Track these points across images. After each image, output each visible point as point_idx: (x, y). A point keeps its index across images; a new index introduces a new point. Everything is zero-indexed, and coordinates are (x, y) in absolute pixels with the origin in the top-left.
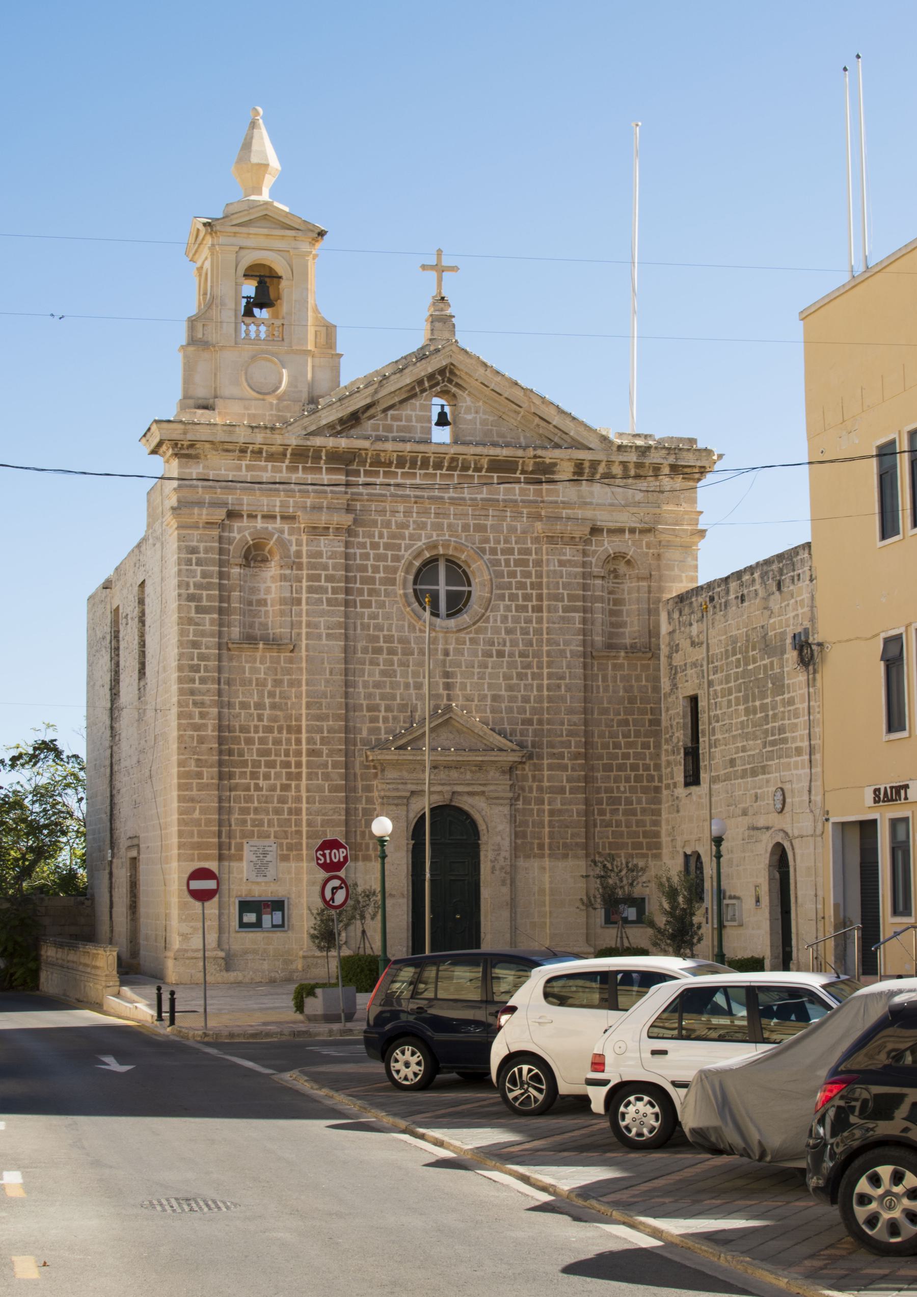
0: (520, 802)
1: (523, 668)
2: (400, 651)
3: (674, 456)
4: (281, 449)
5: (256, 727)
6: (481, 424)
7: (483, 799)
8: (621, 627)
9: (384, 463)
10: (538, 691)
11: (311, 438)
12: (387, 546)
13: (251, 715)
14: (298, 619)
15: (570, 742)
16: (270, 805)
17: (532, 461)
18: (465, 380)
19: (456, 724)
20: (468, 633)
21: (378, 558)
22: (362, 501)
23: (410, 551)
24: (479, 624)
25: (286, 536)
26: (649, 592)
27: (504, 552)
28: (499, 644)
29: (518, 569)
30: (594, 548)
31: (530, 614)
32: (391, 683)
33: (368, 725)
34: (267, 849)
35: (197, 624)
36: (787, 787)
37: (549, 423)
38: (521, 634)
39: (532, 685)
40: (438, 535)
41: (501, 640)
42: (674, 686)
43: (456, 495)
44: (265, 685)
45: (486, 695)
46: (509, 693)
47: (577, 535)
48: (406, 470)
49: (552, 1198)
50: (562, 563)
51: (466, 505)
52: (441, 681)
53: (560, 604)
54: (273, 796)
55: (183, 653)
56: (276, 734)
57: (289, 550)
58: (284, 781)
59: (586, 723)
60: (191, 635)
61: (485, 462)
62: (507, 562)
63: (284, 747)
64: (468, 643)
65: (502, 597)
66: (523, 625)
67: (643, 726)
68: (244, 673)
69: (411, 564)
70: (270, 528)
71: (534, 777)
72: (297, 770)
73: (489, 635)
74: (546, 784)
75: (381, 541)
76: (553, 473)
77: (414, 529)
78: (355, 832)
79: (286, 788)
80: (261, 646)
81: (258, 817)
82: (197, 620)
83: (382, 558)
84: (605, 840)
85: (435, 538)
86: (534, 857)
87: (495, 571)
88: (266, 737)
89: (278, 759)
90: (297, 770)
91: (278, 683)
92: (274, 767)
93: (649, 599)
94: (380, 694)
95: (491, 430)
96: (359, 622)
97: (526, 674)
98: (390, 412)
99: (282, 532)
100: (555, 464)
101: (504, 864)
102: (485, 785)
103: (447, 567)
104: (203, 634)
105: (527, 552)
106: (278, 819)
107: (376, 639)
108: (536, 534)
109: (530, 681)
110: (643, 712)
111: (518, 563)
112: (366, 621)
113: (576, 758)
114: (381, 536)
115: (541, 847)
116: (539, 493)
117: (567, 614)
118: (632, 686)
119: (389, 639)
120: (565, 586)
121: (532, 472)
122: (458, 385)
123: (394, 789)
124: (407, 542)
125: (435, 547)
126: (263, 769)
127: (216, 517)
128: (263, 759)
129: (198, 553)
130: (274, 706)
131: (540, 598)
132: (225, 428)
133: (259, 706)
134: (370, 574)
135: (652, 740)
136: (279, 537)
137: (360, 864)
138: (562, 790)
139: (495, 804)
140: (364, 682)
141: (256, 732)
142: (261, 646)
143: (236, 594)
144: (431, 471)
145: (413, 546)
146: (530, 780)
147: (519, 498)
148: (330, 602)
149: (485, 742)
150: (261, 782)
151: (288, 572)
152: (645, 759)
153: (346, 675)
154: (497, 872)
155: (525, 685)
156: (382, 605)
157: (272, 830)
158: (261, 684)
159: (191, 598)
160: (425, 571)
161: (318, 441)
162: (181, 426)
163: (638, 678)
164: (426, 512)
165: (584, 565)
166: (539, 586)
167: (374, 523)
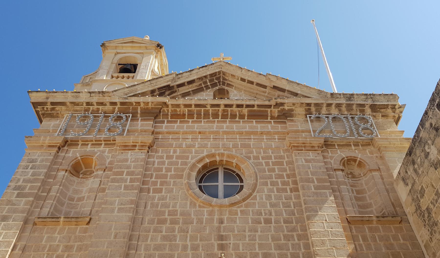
1: (288, 231)
2: (181, 221)
8: (368, 208)
9: (180, 115)
10: (305, 248)
11: (129, 98)
17: (276, 110)
20: (238, 207)
21: (171, 164)
23: (195, 160)
24: (248, 201)
25: (106, 154)
28: (266, 214)
30: (330, 155)
32: (170, 245)
38: (284, 207)
39: (299, 245)
40: (215, 150)
41: (267, 212)
44: (56, 250)
45: (258, 254)
46: (278, 252)
49: (395, 177)
50: (307, 161)
52: (216, 244)
57: (106, 161)
61: (245, 111)
65: (266, 184)
69: (194, 165)
73: (257, 208)
76: (292, 116)
82: (14, 202)
97: (293, 236)
103: (225, 173)
105: (281, 157)
112: (156, 201)
114: (175, 152)
118: (392, 245)
122: (229, 85)
125: (213, 155)
131: (295, 183)
132: (73, 94)
143: (55, 188)
155: (293, 245)
156: (171, 191)
163: (395, 238)
166: (294, 175)
167: (171, 146)
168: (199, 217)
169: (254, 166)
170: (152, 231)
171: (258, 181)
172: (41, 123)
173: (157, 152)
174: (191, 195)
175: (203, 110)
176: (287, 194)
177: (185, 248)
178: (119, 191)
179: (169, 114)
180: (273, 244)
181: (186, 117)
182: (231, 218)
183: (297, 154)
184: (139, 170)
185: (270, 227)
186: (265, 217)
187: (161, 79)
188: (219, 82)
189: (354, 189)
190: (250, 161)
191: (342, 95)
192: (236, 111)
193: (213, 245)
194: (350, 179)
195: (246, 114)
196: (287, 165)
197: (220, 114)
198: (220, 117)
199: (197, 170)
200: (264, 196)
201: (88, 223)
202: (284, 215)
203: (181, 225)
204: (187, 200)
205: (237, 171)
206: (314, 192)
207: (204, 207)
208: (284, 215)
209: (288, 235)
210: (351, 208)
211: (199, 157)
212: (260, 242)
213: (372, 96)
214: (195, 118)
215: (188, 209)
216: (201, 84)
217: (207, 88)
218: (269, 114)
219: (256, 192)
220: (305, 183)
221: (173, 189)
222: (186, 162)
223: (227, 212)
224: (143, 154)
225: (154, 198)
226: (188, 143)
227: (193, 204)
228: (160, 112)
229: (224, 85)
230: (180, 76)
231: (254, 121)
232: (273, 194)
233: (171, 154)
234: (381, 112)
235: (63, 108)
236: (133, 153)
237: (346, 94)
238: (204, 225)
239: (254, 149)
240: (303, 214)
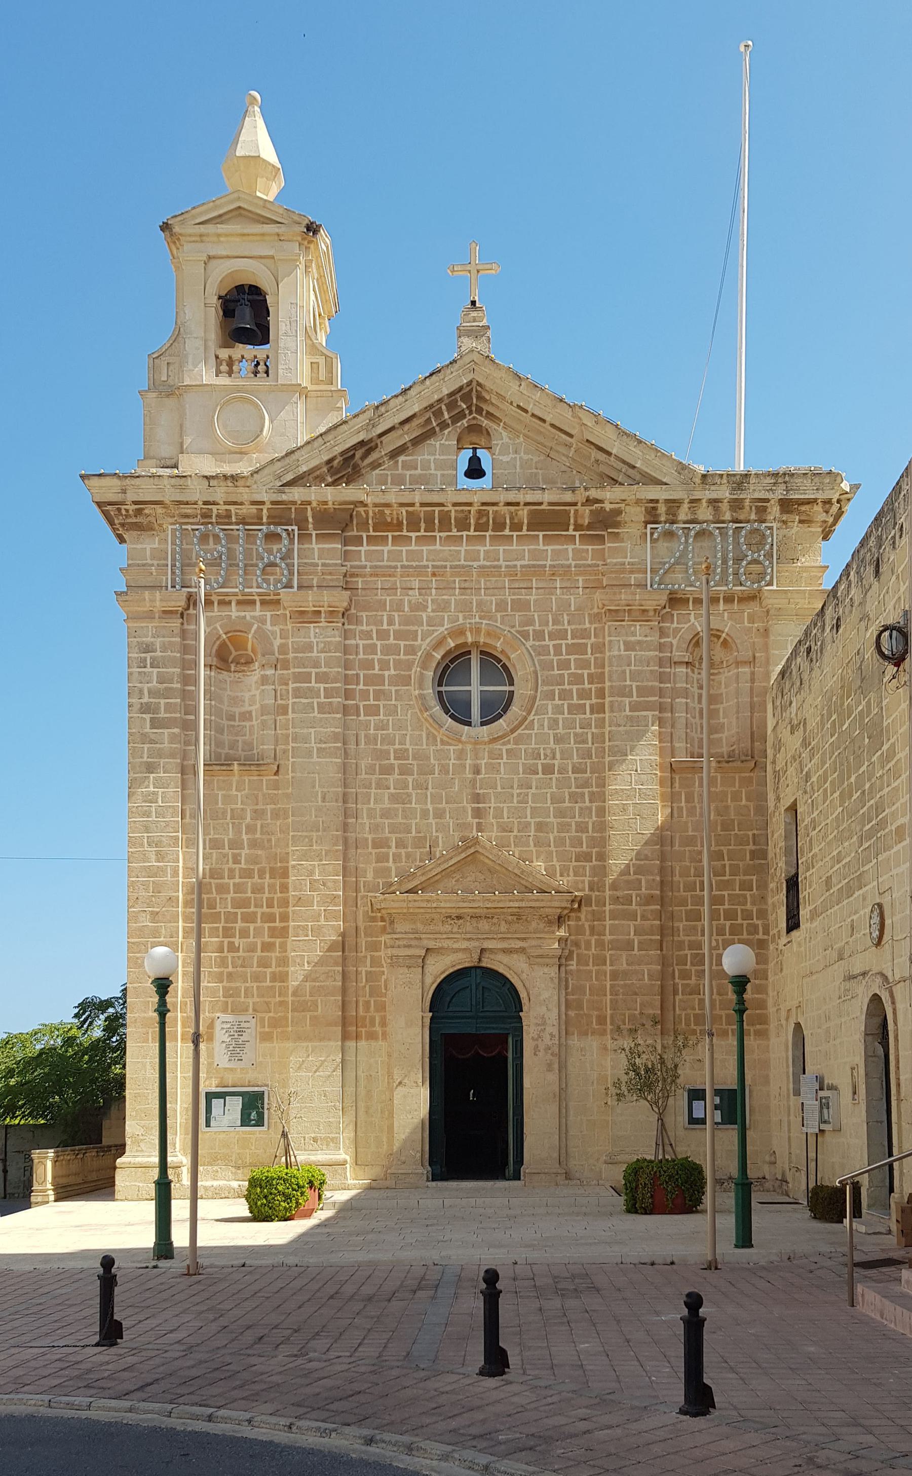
0: (574, 963)
3: (783, 486)
4: (253, 509)
5: (231, 871)
6: (521, 467)
7: (522, 958)
10: (597, 816)
11: (287, 489)
12: (399, 635)
13: (225, 855)
14: (284, 732)
15: (640, 881)
16: (249, 970)
17: (587, 510)
18: (498, 407)
19: (487, 861)
20: (504, 744)
21: (387, 650)
22: (365, 576)
24: (519, 731)
25: (268, 626)
26: (753, 680)
27: (552, 636)
28: (546, 756)
29: (572, 657)
31: (588, 715)
33: (374, 865)
34: (243, 1025)
35: (152, 742)
36: (886, 900)
37: (609, 454)
39: (590, 809)
40: (465, 618)
41: (548, 752)
42: (778, 799)
43: (488, 564)
44: (243, 818)
45: (530, 823)
46: (559, 820)
47: (650, 605)
48: (422, 533)
50: (629, 646)
51: (500, 576)
52: (469, 807)
53: (627, 700)
54: (252, 958)
55: (136, 779)
56: (256, 879)
57: (272, 644)
58: (267, 939)
59: (663, 857)
60: (145, 756)
61: (524, 514)
62: (557, 648)
63: (267, 895)
64: (505, 757)
65: (550, 696)
66: (578, 730)
67: (743, 859)
68: (217, 804)
69: (428, 656)
70: (248, 618)
71: (592, 928)
72: (283, 924)
74: (608, 937)
75: (391, 627)
76: (617, 525)
77: (433, 611)
78: (357, 1002)
79: (267, 947)
80: (236, 767)
81: (233, 985)
82: (153, 737)
83: (396, 650)
84: (689, 1011)
85: (461, 621)
86: (593, 1033)
87: (540, 661)
88: (244, 883)
89: (259, 910)
90: (283, 924)
91: (258, 814)
92: (254, 921)
93: (752, 689)
94: (390, 825)
95: (536, 474)
96: (362, 734)
97: (583, 794)
98: (401, 458)
99: (263, 622)
100: (619, 512)
101: (550, 1043)
102: (524, 939)
104: (160, 754)
105: (585, 634)
106: (258, 987)
107: (385, 754)
108: (596, 610)
109: (587, 804)
110: (742, 841)
111: (571, 649)
113: (647, 903)
114: (391, 622)
115: (601, 1020)
116: (601, 555)
117: (636, 713)
118: (727, 807)
119: (401, 755)
120: (634, 676)
121: (590, 527)
122: (490, 416)
123: (405, 946)
124: (425, 628)
125: (461, 632)
126: (239, 925)
127: (173, 603)
128: (239, 911)
129: (154, 651)
130: (253, 844)
132: (173, 481)
133: (235, 844)
134: (376, 671)
135: (754, 878)
136: (259, 628)
137: (363, 1044)
138: (629, 946)
139: (538, 964)
140: (369, 809)
141: (231, 877)
142: (236, 767)
144: (454, 532)
145: (433, 635)
146: (588, 933)
147: (573, 563)
148: (322, 708)
149: (524, 882)
150: (236, 941)
151: (270, 672)
152: (745, 904)
153: (345, 802)
154: (541, 1054)
156: (393, 711)
157: (250, 1001)
158: (237, 816)
159: (146, 709)
160: (453, 667)
161: (296, 494)
162: (115, 482)
163: (736, 797)
164: (449, 588)
165: (661, 647)
166: (601, 678)
167: (382, 605)
168: (443, 762)
169: (533, 654)
170: (374, 785)
171: (539, 690)
173: (358, 622)
174: (426, 720)
175: (437, 512)
176: (584, 716)
178: (311, 715)
179: (370, 522)
180: (552, 809)
181: (405, 527)
182: (491, 764)
184: (336, 670)
186: (545, 761)
187: (344, 427)
188: (469, 407)
190: (529, 644)
191: (725, 477)
192: (505, 514)
193: (464, 809)
195: (526, 521)
196: (592, 654)
197: (472, 521)
198: (472, 528)
200: (543, 721)
201: (277, 773)
202: (575, 757)
203: (415, 776)
205: (504, 660)
206: (627, 716)
207: (450, 745)
208: (575, 757)
210: (683, 745)
211: (436, 634)
212: (533, 805)
213: (787, 478)
214: (422, 530)
215: (425, 747)
217: (443, 425)
218: (572, 521)
219: (533, 713)
223: (486, 753)
224: (336, 632)
225: (367, 726)
227: (431, 738)
228: (351, 516)
229: (481, 415)
230: (383, 409)
231: (541, 534)
232: (561, 716)
234: (799, 513)
235: (159, 510)
236: (317, 631)
237: (734, 475)
238: (451, 776)
240: (603, 758)
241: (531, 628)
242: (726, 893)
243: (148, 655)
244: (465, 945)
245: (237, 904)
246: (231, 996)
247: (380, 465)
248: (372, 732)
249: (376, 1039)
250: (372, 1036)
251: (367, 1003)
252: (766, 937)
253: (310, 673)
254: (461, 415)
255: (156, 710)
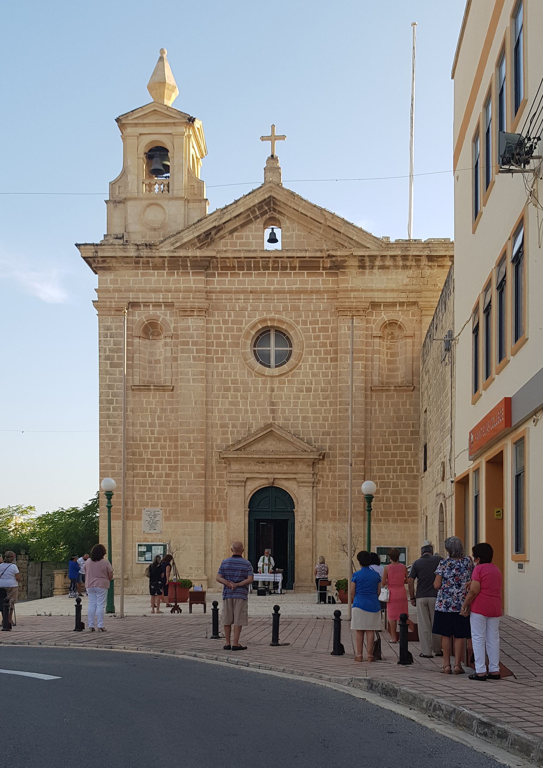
7: (295, 483)
8: (395, 371)
10: (333, 413)
23: (248, 325)
35: (111, 374)
39: (330, 410)
41: (309, 381)
44: (156, 412)
45: (299, 417)
46: (313, 415)
52: (268, 408)
57: (170, 327)
69: (248, 333)
76: (344, 267)
82: (111, 372)
98: (235, 234)
101: (308, 524)
113: (358, 457)
114: (229, 316)
119: (234, 382)
121: (330, 268)
133: (152, 425)
134: (222, 340)
137: (215, 523)
144: (262, 271)
146: (328, 471)
150: (153, 472)
154: (303, 530)
155: (325, 409)
158: (153, 411)
163: (404, 404)
166: (336, 344)
172: (77, 245)
177: (246, 411)
183: (342, 319)
185: (310, 395)
189: (389, 351)
193: (266, 410)
194: (389, 341)
199: (251, 337)
204: (245, 370)
209: (323, 402)
215: (246, 378)
216: (249, 215)
217: (256, 218)
220: (344, 355)
221: (232, 358)
222: (240, 328)
224: (202, 321)
226: (241, 305)
231: (306, 272)
232: (315, 363)
233: (227, 318)
235: (114, 260)
239: (303, 312)
241: (300, 319)
242: (398, 452)
243: (109, 332)
244: (266, 476)
245: (153, 454)
246: (150, 499)
247: (224, 237)
248: (220, 370)
249: (222, 521)
250: (219, 519)
251: (217, 504)
252: (418, 474)
253: (189, 342)
254: (265, 213)
255: (113, 359)
